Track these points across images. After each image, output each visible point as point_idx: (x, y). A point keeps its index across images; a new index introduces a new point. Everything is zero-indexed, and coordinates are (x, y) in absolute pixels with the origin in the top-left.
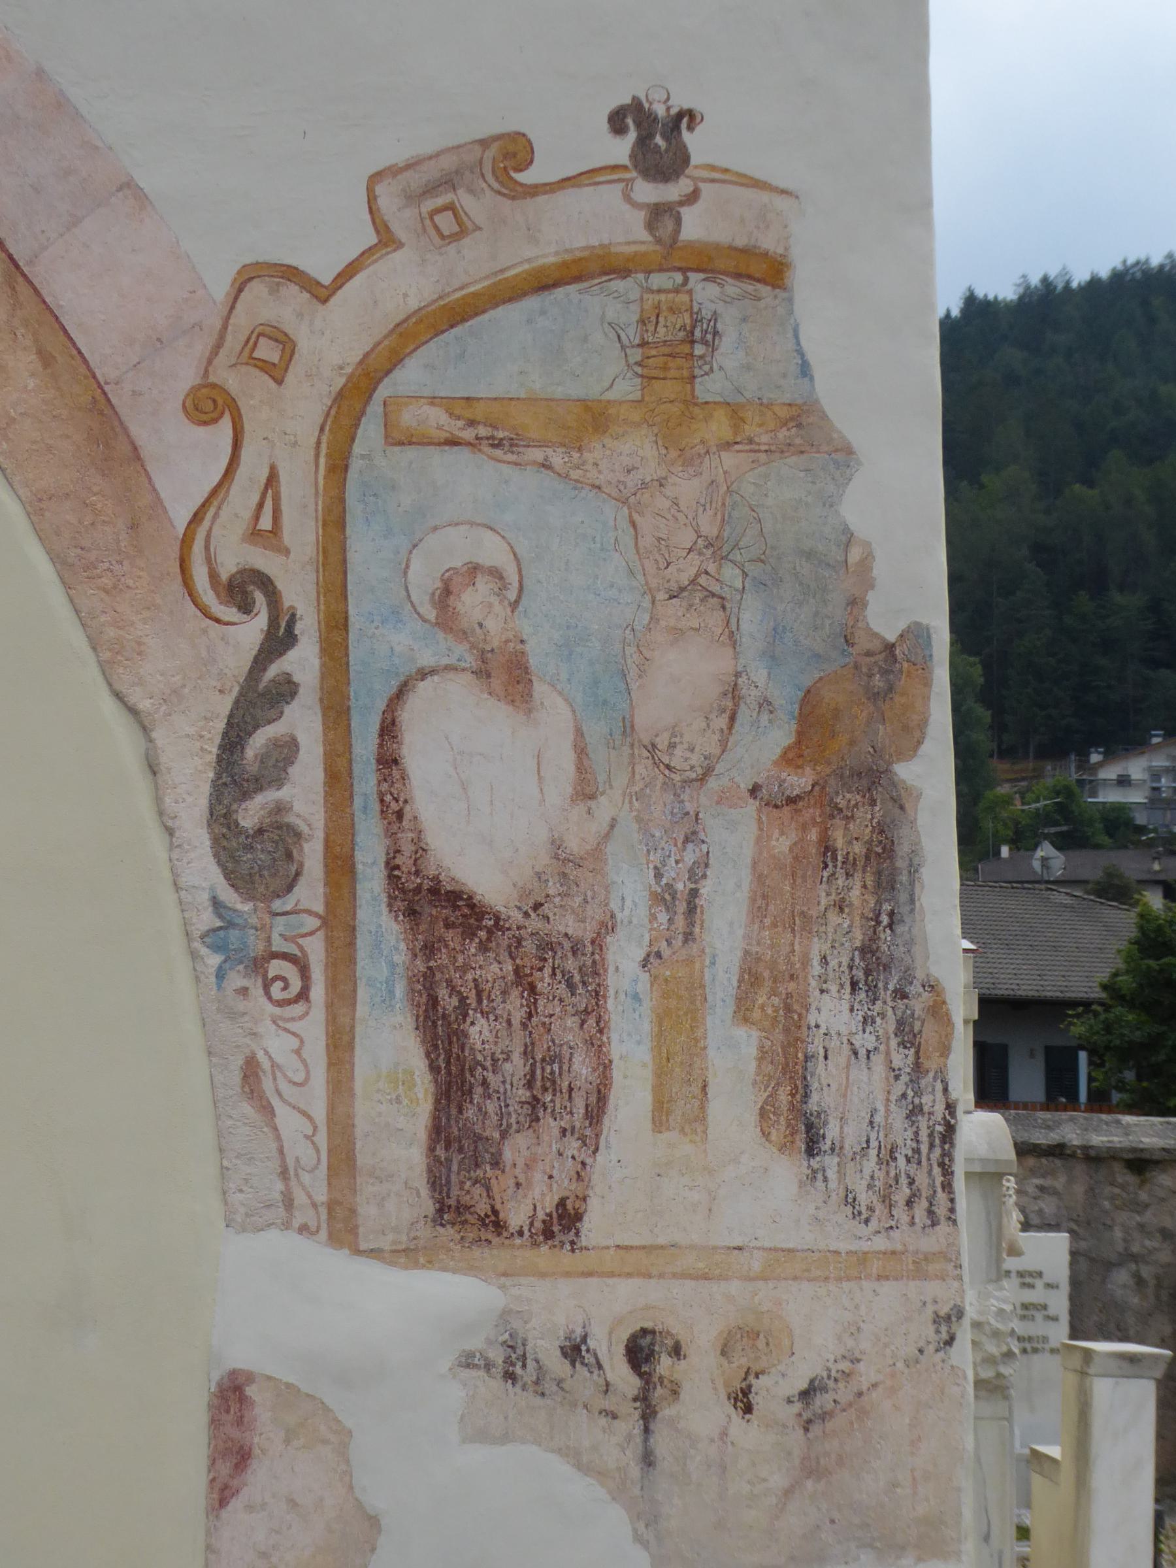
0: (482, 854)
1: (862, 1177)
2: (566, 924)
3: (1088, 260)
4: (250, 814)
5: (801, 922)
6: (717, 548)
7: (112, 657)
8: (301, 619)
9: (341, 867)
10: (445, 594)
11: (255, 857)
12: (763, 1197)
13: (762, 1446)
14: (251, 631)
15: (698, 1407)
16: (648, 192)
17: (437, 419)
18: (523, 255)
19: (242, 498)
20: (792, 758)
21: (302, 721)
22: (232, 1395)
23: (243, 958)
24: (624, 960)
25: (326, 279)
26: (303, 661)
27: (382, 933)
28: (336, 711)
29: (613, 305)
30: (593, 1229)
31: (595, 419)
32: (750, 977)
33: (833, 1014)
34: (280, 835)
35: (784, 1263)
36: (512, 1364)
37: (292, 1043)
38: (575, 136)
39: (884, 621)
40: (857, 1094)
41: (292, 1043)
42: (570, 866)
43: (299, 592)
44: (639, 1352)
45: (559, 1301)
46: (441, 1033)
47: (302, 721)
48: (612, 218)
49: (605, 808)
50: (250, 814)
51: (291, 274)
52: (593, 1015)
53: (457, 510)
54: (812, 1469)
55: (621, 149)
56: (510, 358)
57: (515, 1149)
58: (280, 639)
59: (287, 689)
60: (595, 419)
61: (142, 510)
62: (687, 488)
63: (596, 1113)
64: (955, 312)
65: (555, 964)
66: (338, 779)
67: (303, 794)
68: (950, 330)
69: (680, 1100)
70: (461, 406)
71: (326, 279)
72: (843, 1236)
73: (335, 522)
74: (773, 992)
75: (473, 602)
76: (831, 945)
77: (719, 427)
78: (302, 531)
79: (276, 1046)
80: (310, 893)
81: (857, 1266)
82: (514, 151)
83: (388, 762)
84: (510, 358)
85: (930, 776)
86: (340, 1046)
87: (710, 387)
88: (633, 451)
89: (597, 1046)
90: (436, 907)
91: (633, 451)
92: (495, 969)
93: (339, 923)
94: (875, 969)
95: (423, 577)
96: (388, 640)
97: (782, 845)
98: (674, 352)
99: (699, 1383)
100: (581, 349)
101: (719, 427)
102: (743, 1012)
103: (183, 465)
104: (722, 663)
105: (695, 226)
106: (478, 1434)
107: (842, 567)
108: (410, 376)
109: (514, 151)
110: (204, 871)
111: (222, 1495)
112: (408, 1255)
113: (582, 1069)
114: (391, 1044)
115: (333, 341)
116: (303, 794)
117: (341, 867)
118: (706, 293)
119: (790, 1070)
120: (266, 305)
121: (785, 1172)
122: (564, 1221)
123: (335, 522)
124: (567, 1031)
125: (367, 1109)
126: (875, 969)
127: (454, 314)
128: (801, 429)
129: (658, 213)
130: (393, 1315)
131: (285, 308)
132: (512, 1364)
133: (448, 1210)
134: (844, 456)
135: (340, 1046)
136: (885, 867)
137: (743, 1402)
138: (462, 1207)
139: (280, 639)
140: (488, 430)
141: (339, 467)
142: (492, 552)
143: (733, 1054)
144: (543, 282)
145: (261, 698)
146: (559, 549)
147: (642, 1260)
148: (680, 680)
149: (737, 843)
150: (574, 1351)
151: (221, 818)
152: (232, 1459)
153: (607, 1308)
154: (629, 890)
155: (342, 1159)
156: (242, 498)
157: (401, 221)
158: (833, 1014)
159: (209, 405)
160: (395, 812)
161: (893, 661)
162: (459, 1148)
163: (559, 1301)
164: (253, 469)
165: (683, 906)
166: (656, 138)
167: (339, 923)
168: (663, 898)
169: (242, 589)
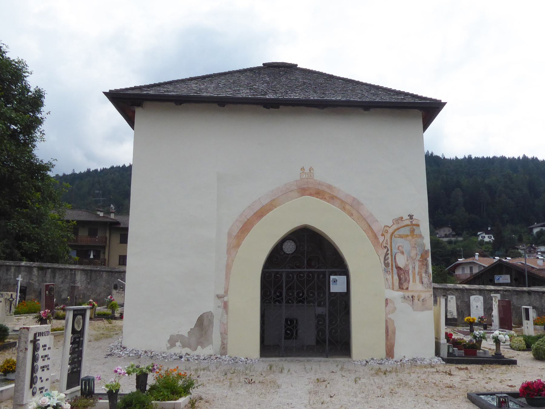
0: (401, 264)
1: (426, 286)
4: (386, 262)
5: (421, 269)
6: (415, 244)
8: (431, 295)
9: (392, 266)
10: (398, 248)
11: (387, 265)
12: (419, 287)
13: (420, 303)
14: (386, 250)
15: (416, 300)
18: (403, 225)
21: (389, 256)
22: (387, 300)
24: (410, 272)
25: (345, 291)
26: (389, 252)
27: (395, 270)
28: (392, 256)
29: (408, 229)
31: (407, 236)
32: (418, 273)
33: (424, 275)
34: (388, 264)
35: (421, 291)
36: (404, 298)
37: (389, 277)
38: (406, 217)
39: (426, 249)
40: (425, 280)
41: (389, 277)
42: (407, 265)
43: (389, 248)
44: (412, 297)
45: (407, 294)
47: (389, 256)
48: (408, 222)
50: (386, 262)
52: (409, 275)
53: (399, 242)
54: (423, 305)
55: (409, 218)
56: (402, 232)
57: (404, 284)
58: (388, 250)
59: (388, 254)
60: (407, 236)
61: (378, 242)
62: (413, 240)
65: (406, 272)
67: (390, 261)
69: (414, 281)
70: (399, 235)
71: (345, 291)
72: (425, 290)
73: (391, 243)
75: (400, 248)
76: (423, 270)
79: (388, 277)
80: (390, 267)
81: (426, 291)
82: (402, 218)
83: (395, 258)
84: (402, 232)
85: (429, 259)
88: (410, 238)
90: (398, 268)
91: (410, 238)
92: (402, 272)
93: (392, 269)
94: (426, 272)
95: (397, 246)
96: (395, 250)
98: (412, 231)
103: (381, 239)
105: (414, 223)
106: (402, 302)
107: (423, 245)
108: (396, 233)
109: (402, 218)
110: (383, 266)
111: (386, 306)
112: (397, 291)
114: (396, 277)
115: (391, 231)
117: (392, 266)
118: (414, 227)
119: (421, 278)
120: (386, 228)
121: (421, 285)
122: (407, 289)
123: (391, 243)
126: (426, 272)
127: (398, 229)
128: (420, 236)
130: (397, 295)
131: (387, 228)
132: (404, 298)
133: (400, 288)
134: (423, 238)
136: (427, 265)
137: (419, 300)
138: (401, 288)
139: (388, 250)
140: (401, 237)
141: (391, 239)
142: (401, 245)
143: (417, 278)
145: (387, 254)
146: (405, 244)
147: (412, 291)
148: (413, 253)
149: (417, 264)
152: (387, 304)
153: (410, 294)
154: (411, 267)
158: (424, 275)
159: (383, 235)
160: (395, 262)
161: (427, 252)
162: (400, 284)
163: (407, 294)
164: (386, 239)
165: (414, 268)
166: (411, 217)
167: (392, 269)
169: (385, 247)
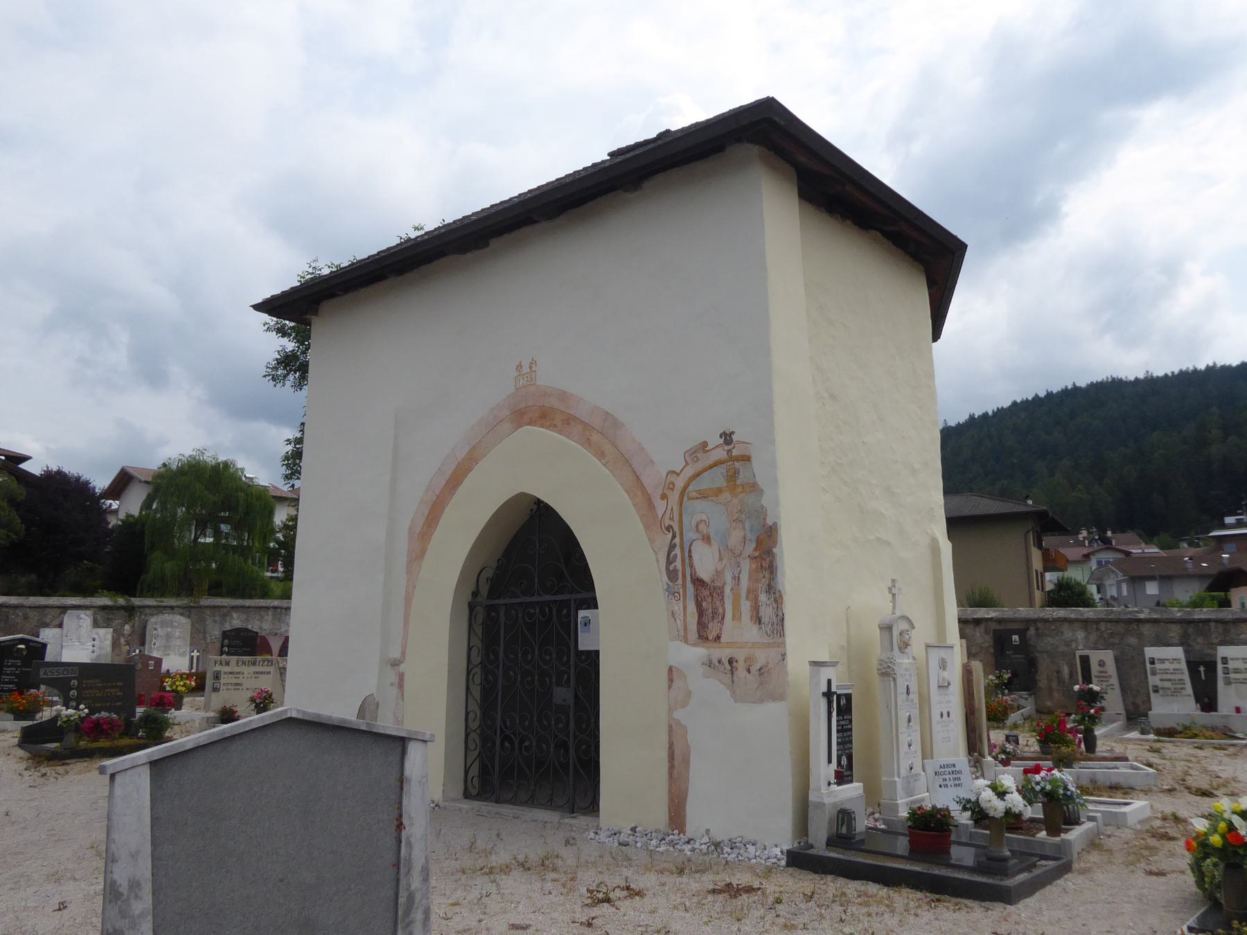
2: (718, 584)
3: (1056, 388)
5: (757, 581)
6: (741, 512)
7: (652, 541)
11: (672, 575)
14: (670, 535)
15: (741, 672)
16: (727, 448)
17: (695, 494)
19: (669, 511)
20: (755, 550)
22: (671, 669)
23: (671, 592)
26: (677, 540)
29: (721, 470)
30: (722, 640)
31: (720, 490)
32: (749, 591)
33: (763, 597)
35: (754, 645)
36: (710, 664)
37: (678, 608)
38: (715, 440)
41: (678, 608)
42: (719, 573)
43: (676, 529)
44: (730, 662)
46: (699, 605)
47: (677, 551)
48: (721, 454)
49: (724, 562)
51: (674, 472)
52: (722, 599)
53: (699, 511)
54: (761, 684)
55: (722, 441)
56: (705, 482)
57: (710, 625)
58: (674, 537)
59: (675, 546)
60: (720, 490)
62: (735, 501)
63: (723, 618)
64: (990, 413)
65: (717, 592)
66: (683, 561)
68: (942, 431)
69: (737, 616)
70: (699, 492)
72: (766, 640)
73: (681, 515)
74: (752, 595)
75: (701, 527)
76: (762, 586)
77: (740, 489)
78: (676, 518)
79: (676, 608)
80: (680, 581)
81: (768, 645)
82: (705, 444)
83: (690, 556)
84: (705, 482)
86: (685, 608)
87: (739, 482)
88: (726, 495)
89: (723, 606)
90: (698, 582)
91: (726, 495)
92: (706, 593)
93: (684, 586)
95: (694, 524)
96: (689, 535)
97: (754, 566)
98: (732, 476)
99: (741, 666)
100: (717, 479)
101: (740, 489)
102: (747, 598)
103: (660, 507)
104: (742, 533)
105: (735, 453)
108: (690, 488)
109: (705, 444)
110: (665, 579)
111: (670, 687)
112: (695, 645)
113: (721, 610)
114: (692, 607)
115: (680, 483)
116: (678, 564)
118: (737, 464)
119: (756, 608)
121: (755, 628)
122: (718, 638)
123: (681, 515)
124: (718, 604)
125: (688, 619)
129: (729, 451)
130: (691, 655)
133: (700, 637)
135: (685, 608)
137: (749, 671)
138: (703, 637)
139: (674, 537)
140: (703, 495)
142: (704, 517)
143: (746, 606)
144: (711, 467)
145: (672, 547)
147: (731, 645)
148: (736, 537)
149: (746, 566)
150: (720, 662)
151: (667, 569)
154: (728, 577)
155: (685, 629)
156: (669, 511)
157: (689, 460)
158: (763, 597)
159: (664, 496)
160: (691, 566)
162: (702, 625)
165: (737, 579)
166: (727, 437)
168: (734, 578)
169: (669, 528)
